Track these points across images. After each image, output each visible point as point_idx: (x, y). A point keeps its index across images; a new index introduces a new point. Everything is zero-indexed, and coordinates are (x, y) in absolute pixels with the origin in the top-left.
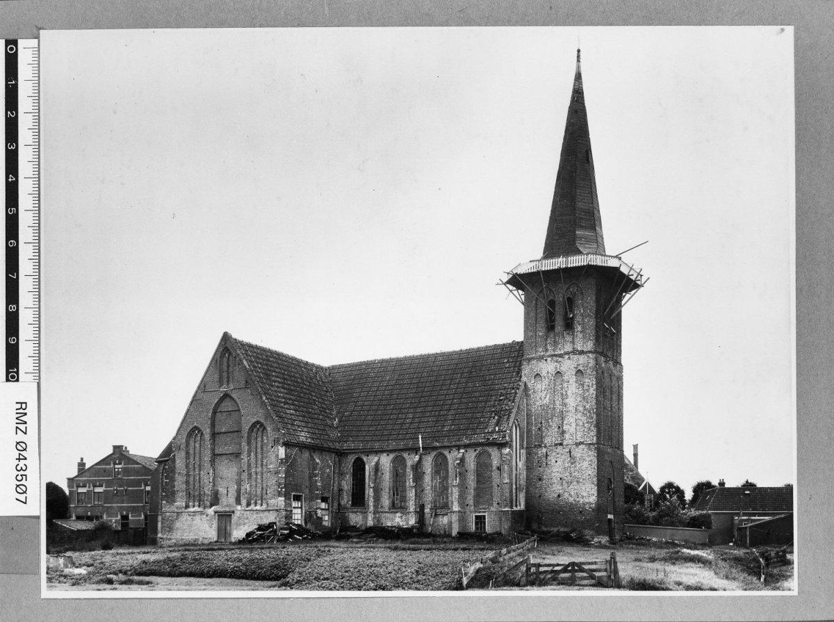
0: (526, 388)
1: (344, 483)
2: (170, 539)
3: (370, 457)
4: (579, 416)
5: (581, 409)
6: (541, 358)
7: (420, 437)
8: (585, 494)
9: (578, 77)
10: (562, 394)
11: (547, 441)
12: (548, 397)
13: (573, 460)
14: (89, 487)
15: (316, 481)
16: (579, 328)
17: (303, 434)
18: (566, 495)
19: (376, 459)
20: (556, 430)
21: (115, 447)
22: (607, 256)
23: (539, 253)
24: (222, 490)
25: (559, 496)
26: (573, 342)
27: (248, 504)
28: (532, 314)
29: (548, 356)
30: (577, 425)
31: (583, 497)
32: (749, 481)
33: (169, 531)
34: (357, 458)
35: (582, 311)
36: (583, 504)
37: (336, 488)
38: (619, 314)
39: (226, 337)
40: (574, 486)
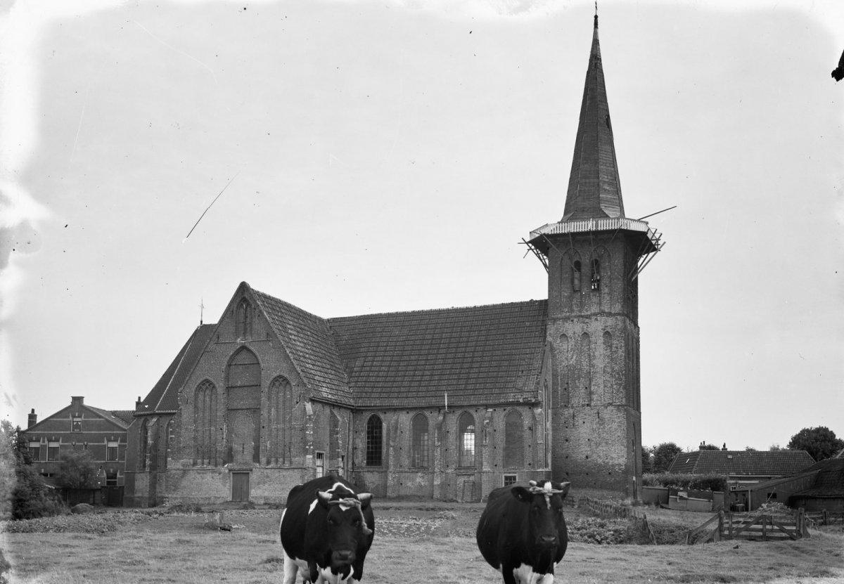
0: (552, 349)
1: (358, 441)
2: (176, 498)
3: (387, 415)
4: (607, 377)
5: (609, 370)
6: (566, 319)
7: (446, 395)
8: (614, 456)
9: (596, 42)
10: (589, 355)
11: (574, 401)
12: (574, 357)
13: (601, 421)
14: (44, 442)
15: (337, 439)
16: (606, 290)
17: (324, 389)
18: (595, 456)
19: (395, 417)
20: (583, 391)
21: (74, 398)
22: (626, 219)
23: (560, 215)
24: (236, 447)
25: (587, 457)
26: (600, 304)
27: (268, 463)
28: (557, 275)
29: (575, 317)
30: (605, 386)
31: (612, 458)
32: (86, 403)
33: (174, 490)
34: (373, 416)
35: (609, 273)
36: (612, 465)
37: (350, 447)
38: (637, 279)
39: (243, 287)
40: (603, 448)
